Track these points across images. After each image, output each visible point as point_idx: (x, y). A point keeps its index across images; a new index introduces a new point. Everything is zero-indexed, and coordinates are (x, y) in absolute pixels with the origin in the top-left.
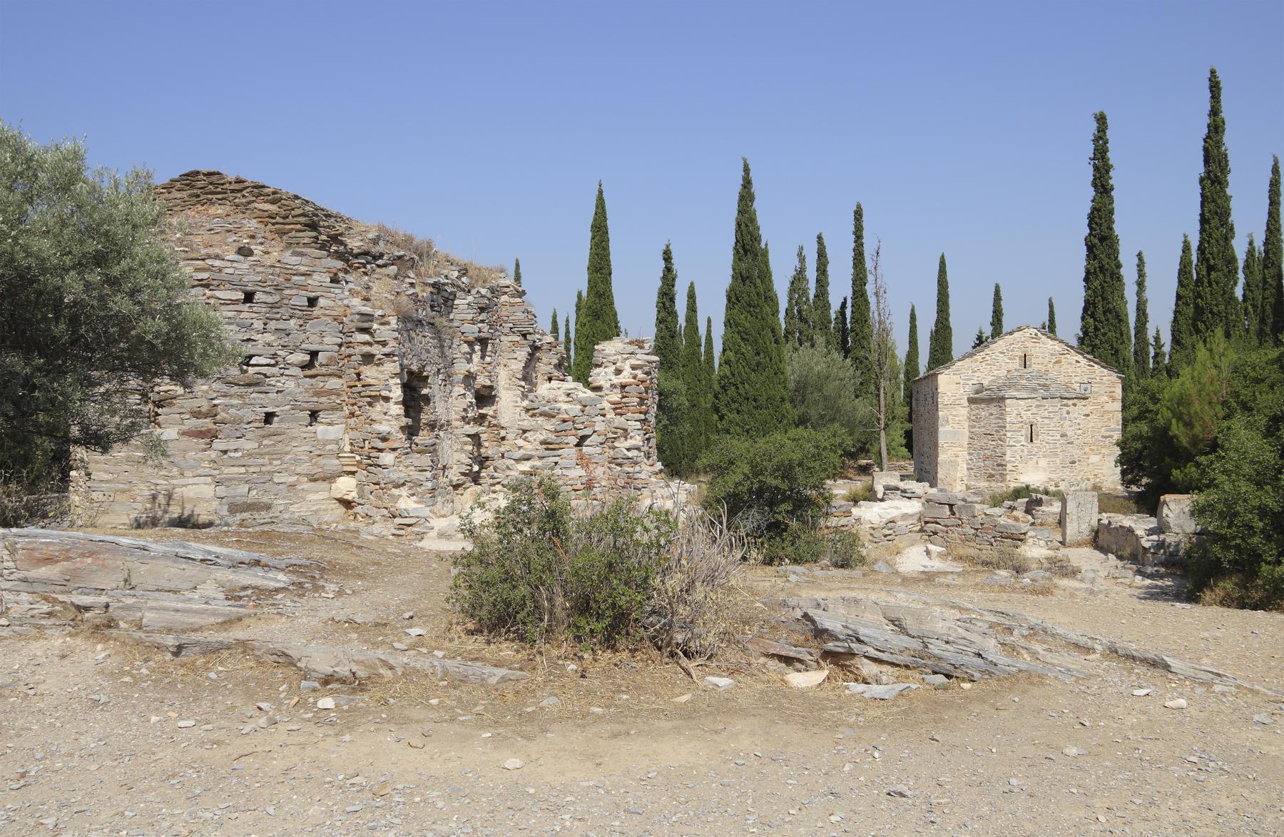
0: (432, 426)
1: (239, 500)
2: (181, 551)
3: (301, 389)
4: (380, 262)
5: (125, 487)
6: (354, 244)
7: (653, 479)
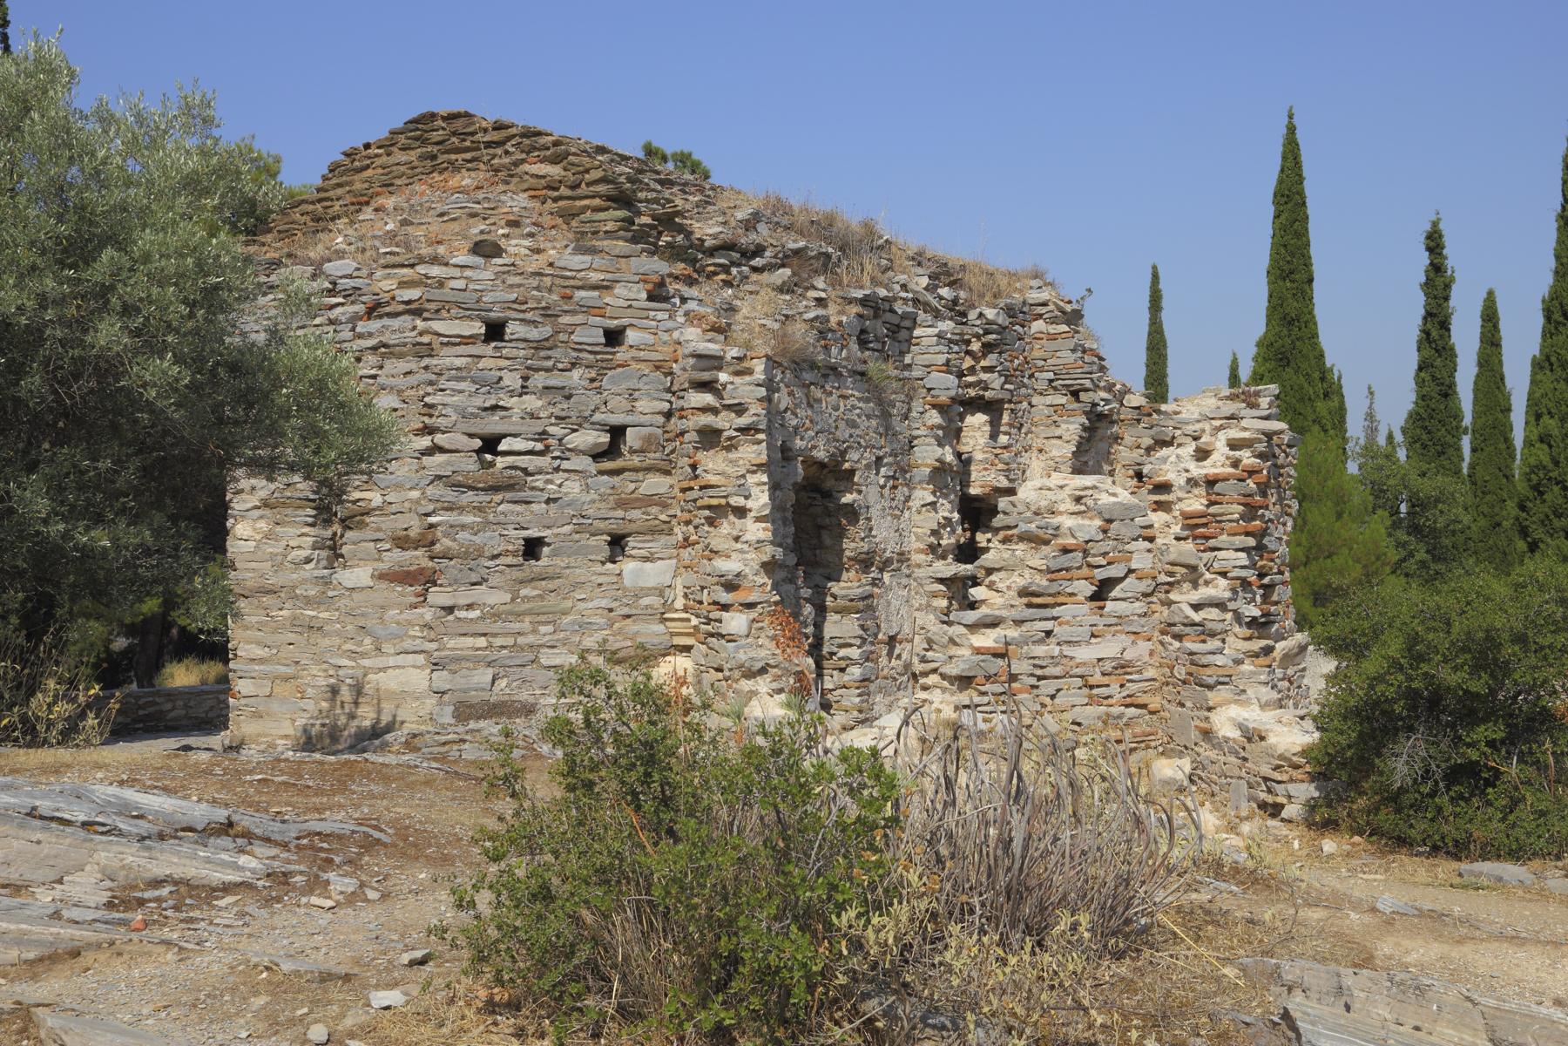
0: (865, 562)
1: (474, 697)
3: (593, 495)
5: (290, 671)
6: (707, 229)
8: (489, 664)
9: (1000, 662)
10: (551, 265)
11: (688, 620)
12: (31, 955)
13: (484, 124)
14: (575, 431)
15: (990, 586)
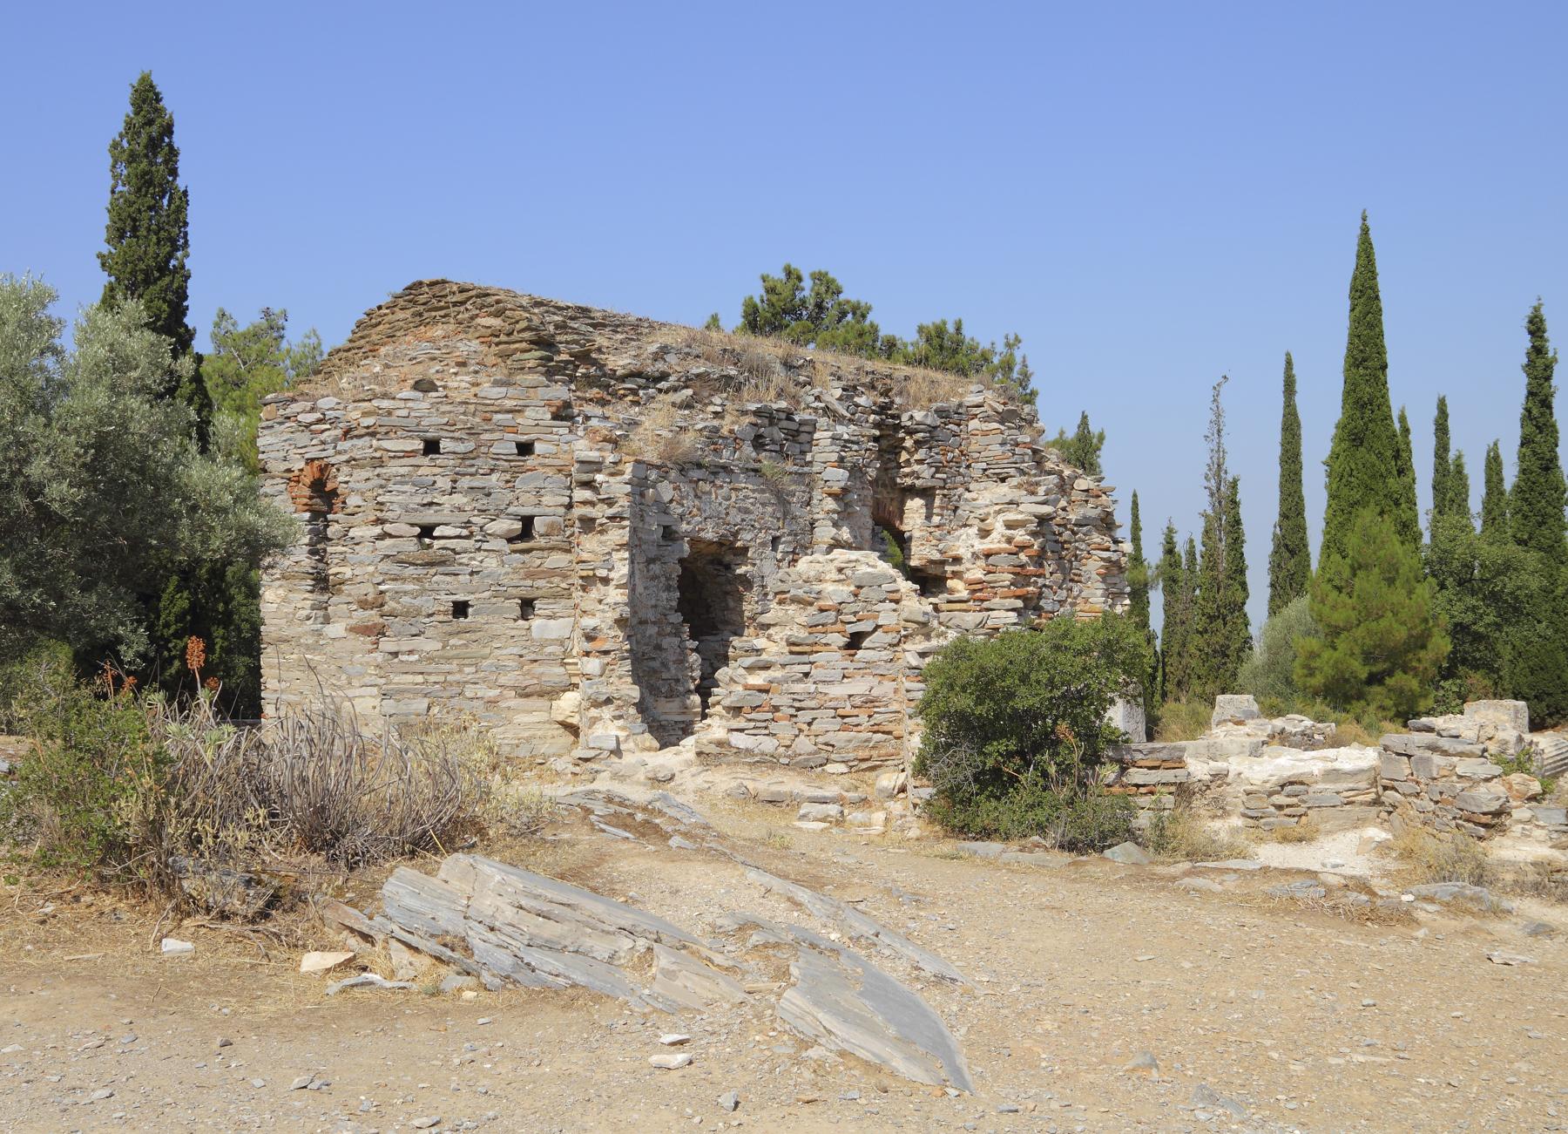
3: (507, 569)
4: (663, 385)
6: (619, 362)
8: (425, 696)
9: (764, 696)
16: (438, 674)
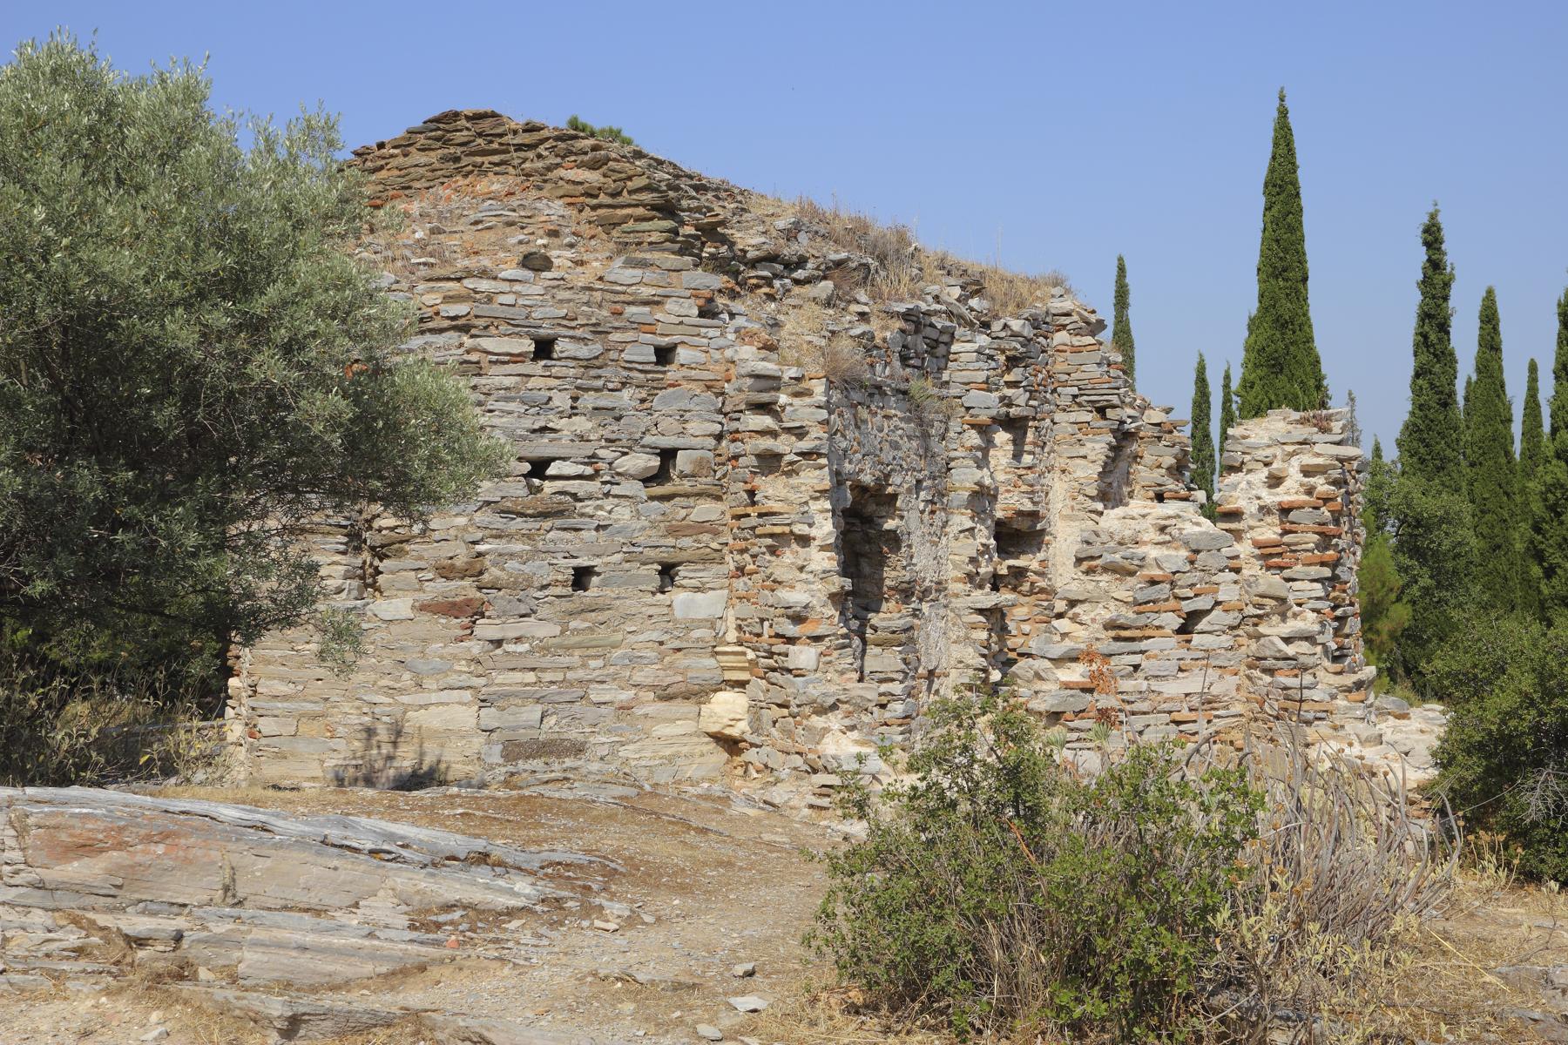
0: (906, 592)
1: (524, 735)
2: (335, 834)
4: (800, 274)
5: (317, 708)
6: (749, 240)
7: (1341, 702)
8: (538, 701)
10: (601, 279)
11: (744, 654)
12: (384, 970)
13: (513, 126)
14: (625, 454)
15: (1073, 619)
16: (555, 669)
